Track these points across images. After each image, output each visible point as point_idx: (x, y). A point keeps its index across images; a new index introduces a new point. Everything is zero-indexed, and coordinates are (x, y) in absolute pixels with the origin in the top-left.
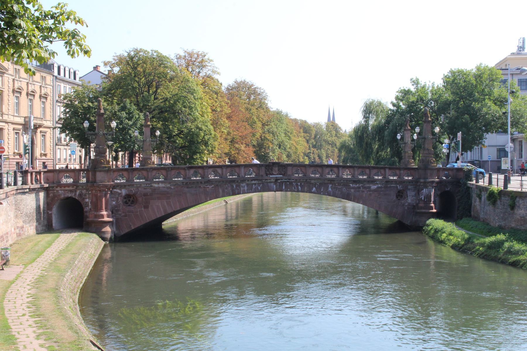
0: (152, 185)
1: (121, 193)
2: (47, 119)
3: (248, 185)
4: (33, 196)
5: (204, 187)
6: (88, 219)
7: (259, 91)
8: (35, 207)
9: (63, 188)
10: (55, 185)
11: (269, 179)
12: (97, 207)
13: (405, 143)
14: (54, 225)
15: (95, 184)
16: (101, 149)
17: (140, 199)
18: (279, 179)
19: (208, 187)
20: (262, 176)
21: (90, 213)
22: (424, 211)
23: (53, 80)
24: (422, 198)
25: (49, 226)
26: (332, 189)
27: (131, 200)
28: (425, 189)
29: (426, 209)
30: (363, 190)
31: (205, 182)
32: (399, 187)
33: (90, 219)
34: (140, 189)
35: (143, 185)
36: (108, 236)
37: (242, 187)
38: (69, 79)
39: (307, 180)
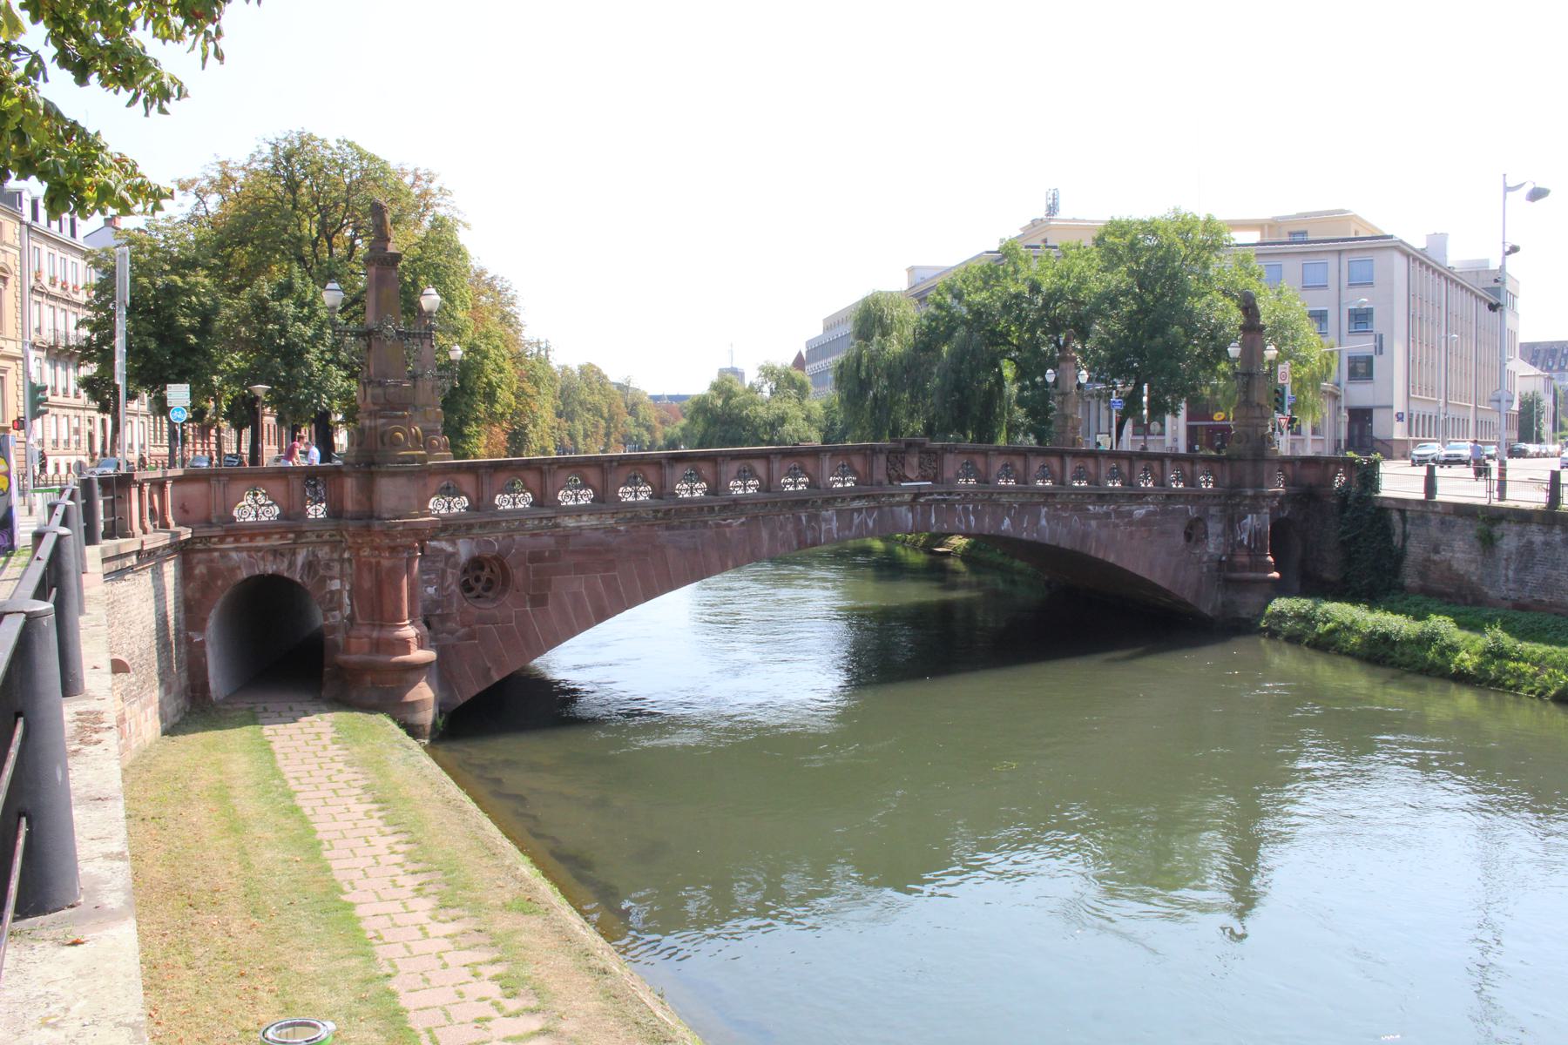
0: (558, 521)
1: (453, 555)
2: (8, 336)
3: (839, 513)
4: (146, 578)
5: (718, 525)
6: (342, 658)
7: (498, 285)
8: (154, 626)
9: (245, 543)
10: (217, 531)
11: (899, 495)
12: (379, 610)
13: (1064, 394)
14: (212, 685)
15: (377, 526)
16: (392, 390)
17: (518, 574)
18: (925, 494)
19: (729, 525)
20: (880, 483)
21: (354, 633)
22: (1252, 575)
23: (20, 234)
24: (1242, 541)
25: (193, 691)
26: (1048, 521)
27: (483, 579)
28: (1250, 516)
29: (1256, 571)
30: (1117, 521)
31: (724, 508)
32: (1192, 511)
33: (354, 658)
34: (517, 537)
35: (529, 524)
36: (427, 716)
37: (825, 520)
38: (60, 235)
39: (992, 494)
